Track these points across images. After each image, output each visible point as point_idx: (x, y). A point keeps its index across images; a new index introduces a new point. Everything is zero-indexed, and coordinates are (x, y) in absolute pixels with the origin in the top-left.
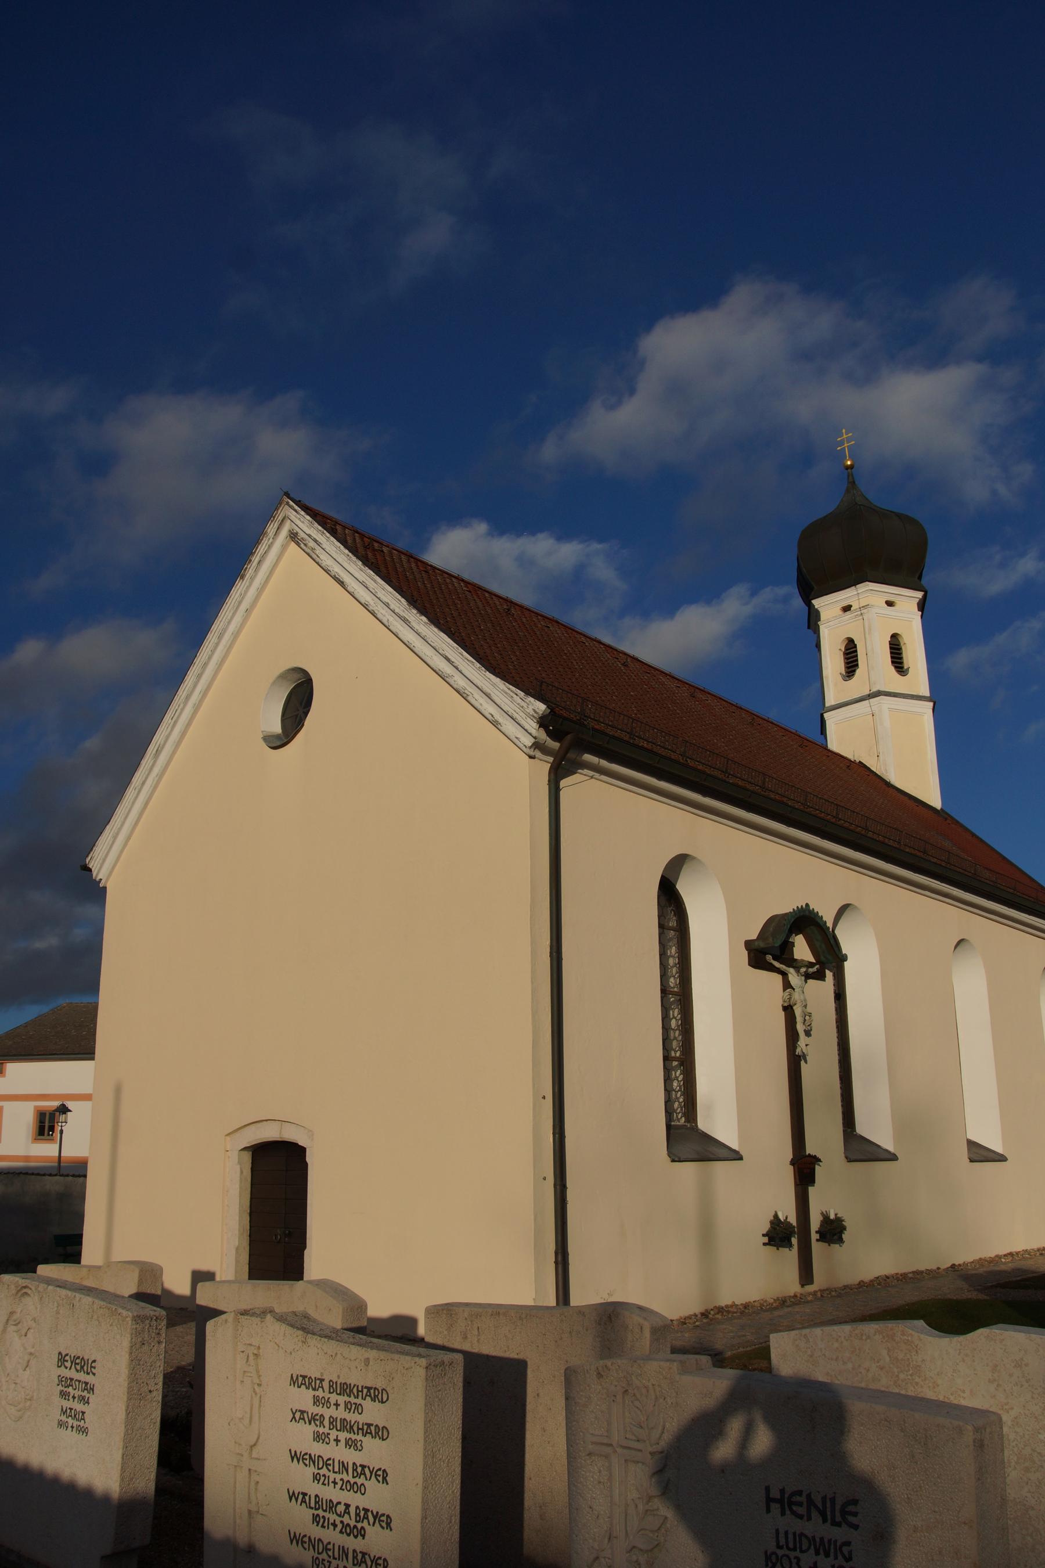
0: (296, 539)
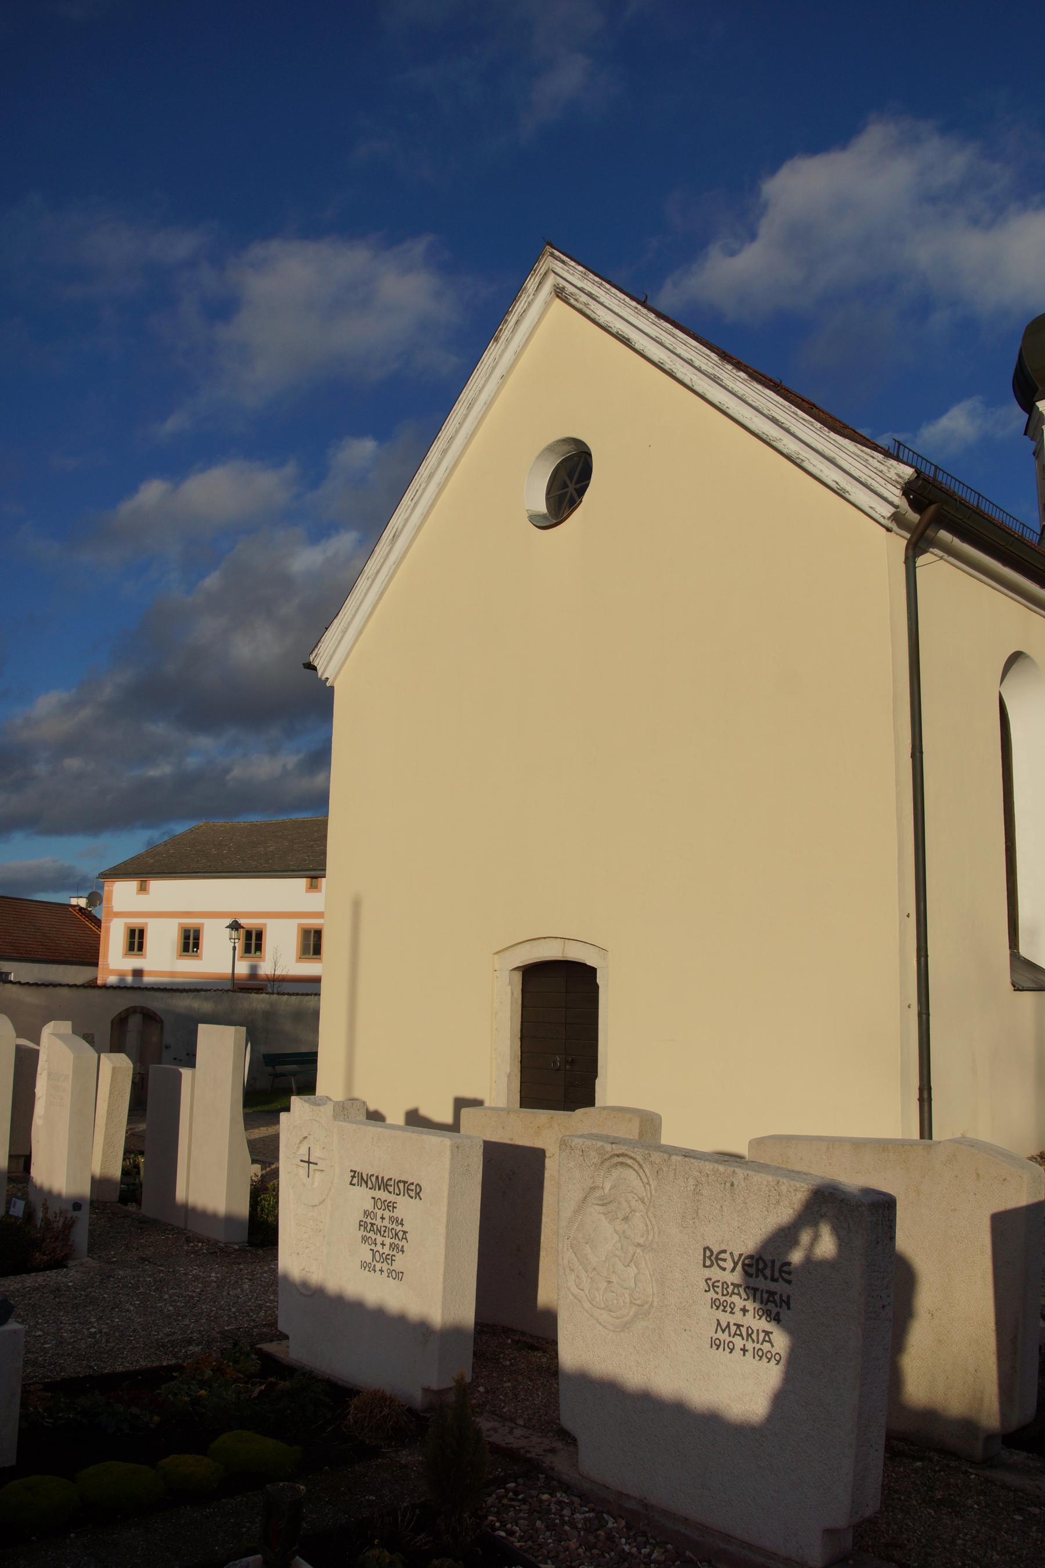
0: (564, 293)
